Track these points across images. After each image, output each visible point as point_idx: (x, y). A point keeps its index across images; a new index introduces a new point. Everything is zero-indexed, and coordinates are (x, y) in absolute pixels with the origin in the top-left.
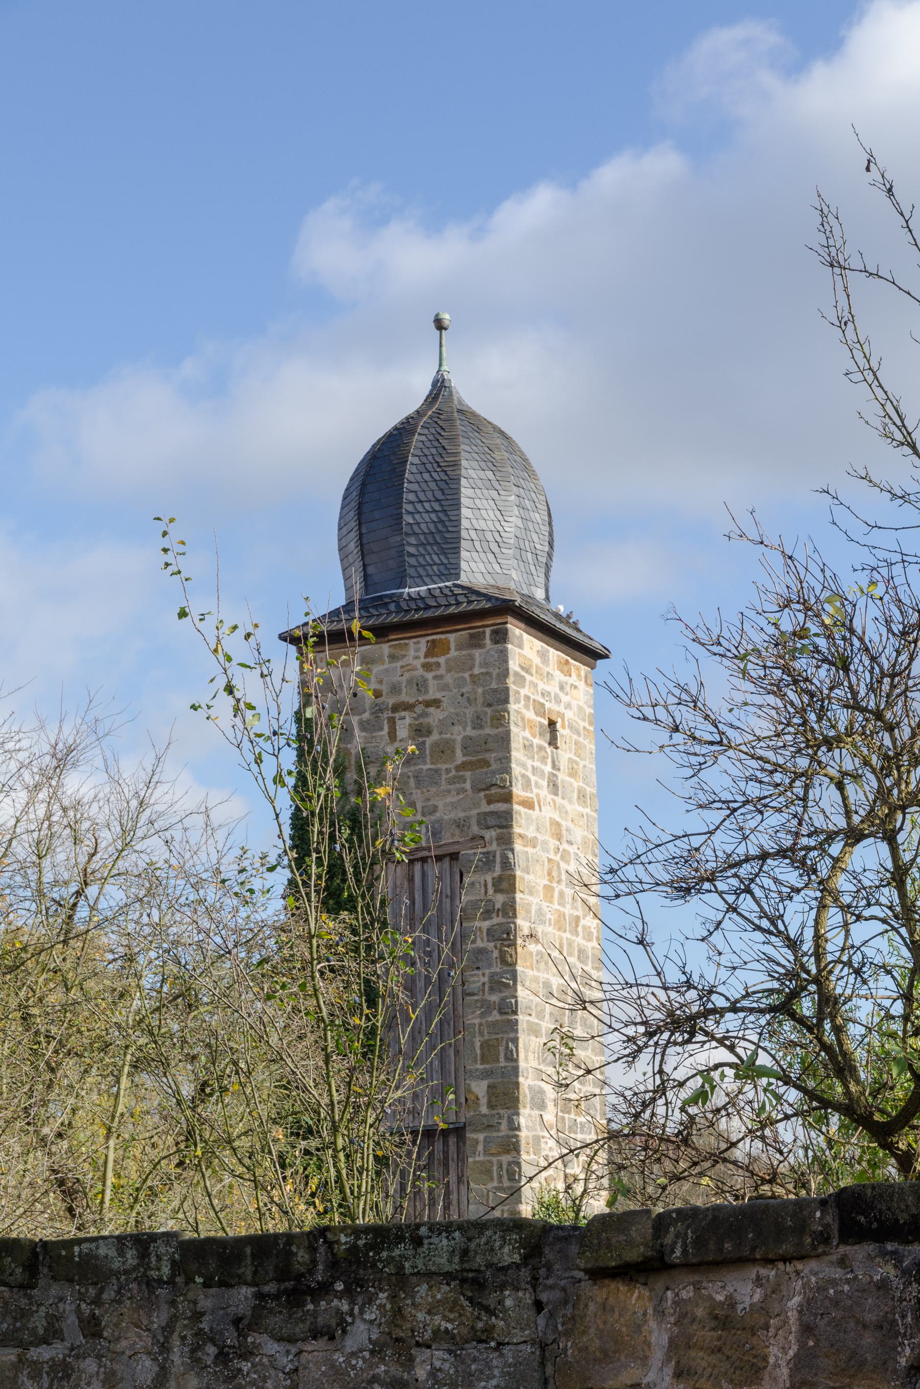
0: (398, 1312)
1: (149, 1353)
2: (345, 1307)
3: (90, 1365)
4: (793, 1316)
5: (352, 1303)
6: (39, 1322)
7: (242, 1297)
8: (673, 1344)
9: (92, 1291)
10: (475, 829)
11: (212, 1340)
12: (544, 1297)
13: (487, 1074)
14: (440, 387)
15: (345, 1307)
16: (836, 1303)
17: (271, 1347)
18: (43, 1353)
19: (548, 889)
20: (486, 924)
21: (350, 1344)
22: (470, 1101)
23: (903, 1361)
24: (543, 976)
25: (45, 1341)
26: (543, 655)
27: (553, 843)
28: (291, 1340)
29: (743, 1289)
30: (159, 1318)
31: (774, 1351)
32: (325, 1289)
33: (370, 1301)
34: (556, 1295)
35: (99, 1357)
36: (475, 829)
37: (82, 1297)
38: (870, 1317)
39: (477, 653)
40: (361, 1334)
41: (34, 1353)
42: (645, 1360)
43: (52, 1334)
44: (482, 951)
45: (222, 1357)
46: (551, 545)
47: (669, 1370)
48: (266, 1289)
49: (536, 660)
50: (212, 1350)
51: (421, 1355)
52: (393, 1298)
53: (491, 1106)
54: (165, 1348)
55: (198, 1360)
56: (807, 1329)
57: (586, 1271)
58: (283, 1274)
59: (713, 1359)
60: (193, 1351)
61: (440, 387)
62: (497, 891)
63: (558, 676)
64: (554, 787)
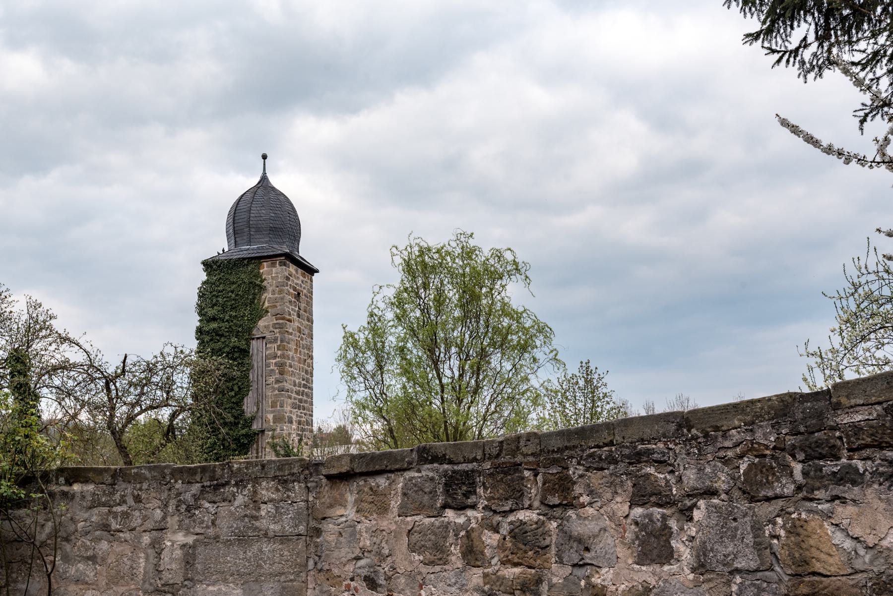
0: (255, 492)
1: (159, 508)
2: (235, 490)
3: (137, 513)
4: (399, 490)
5: (238, 489)
6: (117, 497)
7: (195, 488)
8: (356, 501)
9: (138, 486)
10: (272, 329)
11: (184, 503)
12: (309, 485)
13: (272, 412)
14: (264, 179)
15: (235, 490)
16: (415, 485)
17: (207, 505)
18: (119, 509)
19: (296, 350)
20: (274, 361)
21: (236, 503)
22: (267, 421)
23: (439, 505)
24: (293, 379)
25: (119, 504)
26: (297, 271)
27: (298, 334)
28: (214, 502)
29: (382, 481)
30: (164, 496)
31: (393, 502)
32: (227, 483)
33: (245, 487)
34: (314, 484)
35: (140, 510)
36: (272, 329)
37: (134, 489)
38: (427, 490)
39: (274, 269)
40: (240, 500)
41: (114, 509)
42: (345, 507)
43: (123, 501)
44: (272, 370)
45: (188, 510)
46: (829, 150)
47: (354, 510)
48: (205, 484)
49: (294, 272)
50: (184, 506)
51: (263, 506)
52: (253, 486)
53: (274, 422)
54: (166, 506)
55: (179, 510)
56: (405, 494)
57: (325, 476)
58: (212, 478)
59: (370, 506)
60: (177, 507)
61: (264, 179)
62: (278, 349)
63: (301, 278)
64: (299, 316)
